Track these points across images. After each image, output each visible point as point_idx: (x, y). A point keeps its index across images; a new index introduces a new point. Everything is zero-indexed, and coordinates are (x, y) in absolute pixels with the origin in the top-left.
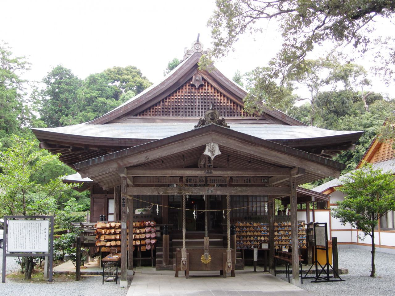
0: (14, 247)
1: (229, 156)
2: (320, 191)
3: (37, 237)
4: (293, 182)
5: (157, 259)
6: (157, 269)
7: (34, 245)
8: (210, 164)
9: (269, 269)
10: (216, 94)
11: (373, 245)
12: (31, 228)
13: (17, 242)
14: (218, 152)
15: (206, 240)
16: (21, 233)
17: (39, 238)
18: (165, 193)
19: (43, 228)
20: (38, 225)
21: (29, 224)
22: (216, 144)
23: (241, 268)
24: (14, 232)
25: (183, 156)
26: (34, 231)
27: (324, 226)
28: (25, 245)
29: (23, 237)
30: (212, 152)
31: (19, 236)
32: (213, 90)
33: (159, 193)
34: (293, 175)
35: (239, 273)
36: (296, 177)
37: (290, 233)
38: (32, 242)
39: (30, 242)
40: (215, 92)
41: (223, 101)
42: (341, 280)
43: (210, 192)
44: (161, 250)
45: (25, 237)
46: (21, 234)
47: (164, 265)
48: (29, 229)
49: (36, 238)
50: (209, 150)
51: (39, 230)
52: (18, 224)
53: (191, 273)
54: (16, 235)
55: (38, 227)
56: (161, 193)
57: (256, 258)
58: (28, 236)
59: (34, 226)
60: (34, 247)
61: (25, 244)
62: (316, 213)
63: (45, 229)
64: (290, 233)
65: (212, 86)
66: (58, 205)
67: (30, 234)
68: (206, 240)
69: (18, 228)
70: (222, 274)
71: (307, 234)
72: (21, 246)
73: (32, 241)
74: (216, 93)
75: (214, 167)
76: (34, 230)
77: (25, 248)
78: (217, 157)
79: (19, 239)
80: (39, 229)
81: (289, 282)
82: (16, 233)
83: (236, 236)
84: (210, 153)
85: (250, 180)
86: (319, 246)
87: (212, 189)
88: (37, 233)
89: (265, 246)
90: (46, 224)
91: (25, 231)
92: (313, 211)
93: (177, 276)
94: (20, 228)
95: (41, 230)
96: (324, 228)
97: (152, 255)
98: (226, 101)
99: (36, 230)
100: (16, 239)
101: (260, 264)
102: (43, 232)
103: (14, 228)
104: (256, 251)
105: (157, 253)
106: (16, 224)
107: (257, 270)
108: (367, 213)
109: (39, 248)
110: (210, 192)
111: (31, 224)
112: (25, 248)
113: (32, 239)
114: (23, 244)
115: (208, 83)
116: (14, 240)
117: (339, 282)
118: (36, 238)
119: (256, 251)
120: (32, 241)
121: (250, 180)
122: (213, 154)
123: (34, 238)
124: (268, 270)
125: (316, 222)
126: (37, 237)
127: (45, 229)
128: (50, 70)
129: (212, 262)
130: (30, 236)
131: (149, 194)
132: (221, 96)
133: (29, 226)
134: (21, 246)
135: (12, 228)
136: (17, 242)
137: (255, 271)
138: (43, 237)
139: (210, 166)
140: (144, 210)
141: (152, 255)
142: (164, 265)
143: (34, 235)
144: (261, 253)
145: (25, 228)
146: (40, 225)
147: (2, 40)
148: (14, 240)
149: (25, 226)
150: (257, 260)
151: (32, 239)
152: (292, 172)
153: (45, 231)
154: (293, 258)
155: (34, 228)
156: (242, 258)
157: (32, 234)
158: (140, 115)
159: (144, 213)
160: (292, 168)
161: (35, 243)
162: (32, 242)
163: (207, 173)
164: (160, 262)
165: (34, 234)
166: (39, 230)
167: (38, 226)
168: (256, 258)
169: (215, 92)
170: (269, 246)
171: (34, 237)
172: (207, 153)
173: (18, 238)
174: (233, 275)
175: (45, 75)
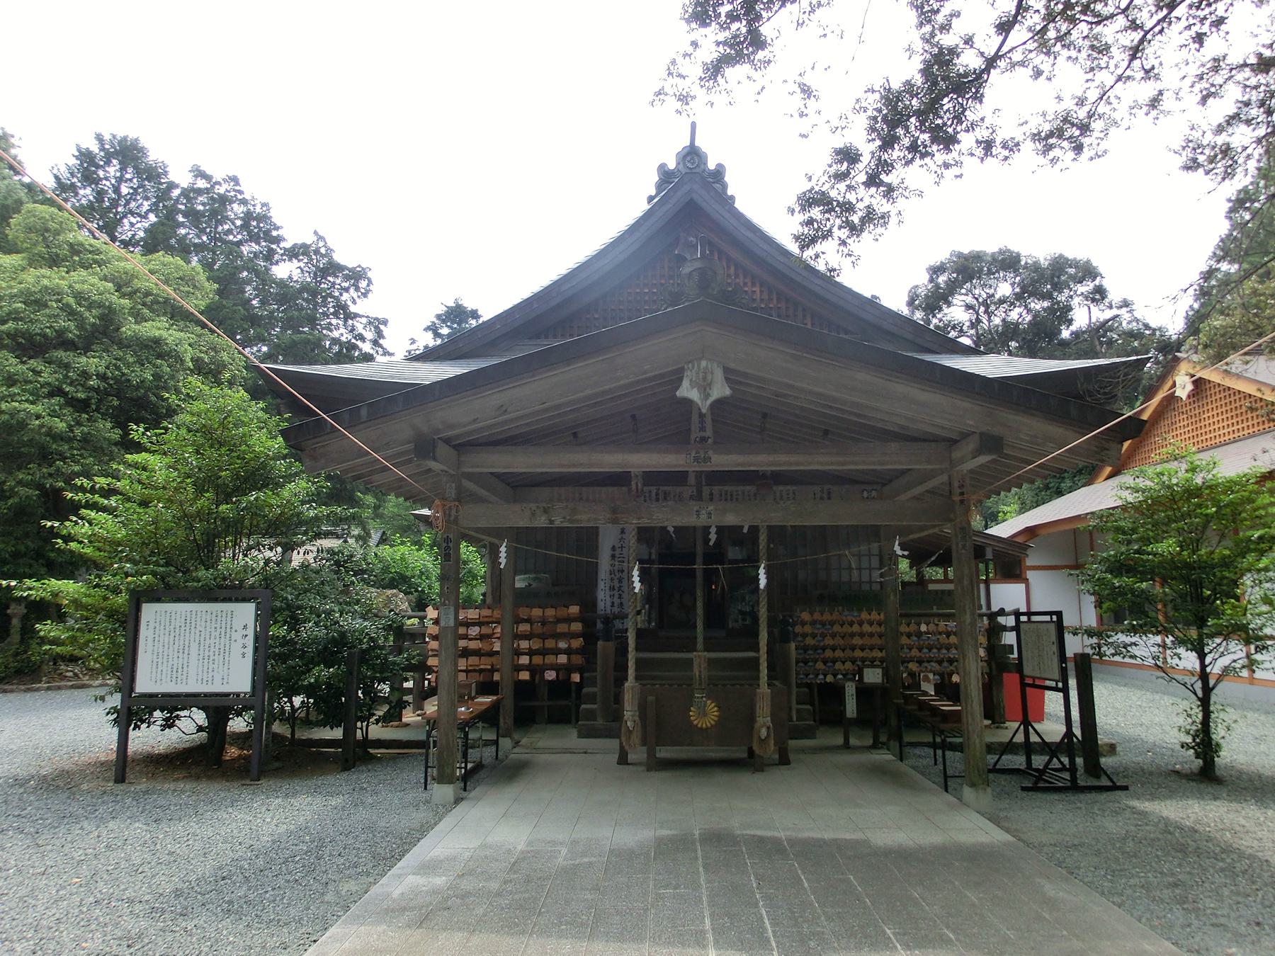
1: (765, 415)
2: (1005, 535)
4: (961, 486)
5: (583, 706)
6: (581, 735)
8: (703, 434)
9: (889, 740)
10: (740, 280)
11: (1204, 676)
14: (720, 390)
15: (700, 658)
18: (570, 521)
19: (238, 625)
22: (715, 365)
23: (807, 733)
25: (633, 417)
27: (1052, 621)
30: (705, 388)
32: (732, 269)
33: (551, 522)
34: (962, 461)
35: (802, 750)
36: (971, 471)
37: (953, 639)
40: (737, 276)
41: (757, 296)
42: (1114, 788)
43: (704, 516)
44: (594, 684)
47: (600, 722)
50: (693, 384)
53: (664, 753)
56: (558, 522)
57: (851, 708)
58: (194, 646)
62: (993, 587)
63: (245, 627)
64: (953, 639)
65: (729, 259)
68: (700, 658)
70: (751, 763)
71: (989, 640)
74: (741, 277)
75: (715, 442)
78: (719, 403)
81: (946, 791)
83: (793, 645)
84: (695, 390)
85: (829, 493)
86: (1034, 678)
87: (711, 508)
89: (873, 676)
90: (245, 613)
92: (987, 582)
93: (623, 760)
96: (1052, 628)
97: (574, 695)
98: (765, 296)
101: (861, 722)
104: (850, 689)
105: (585, 690)
107: (853, 741)
108: (1175, 581)
110: (704, 516)
115: (720, 252)
117: (1104, 796)
119: (850, 689)
121: (829, 493)
122: (707, 396)
124: (883, 739)
125: (995, 608)
127: (245, 627)
128: (441, 310)
129: (721, 722)
131: (521, 524)
132: (753, 284)
135: (152, 625)
137: (846, 746)
138: (236, 649)
139: (703, 440)
140: (535, 579)
141: (574, 695)
142: (600, 722)
144: (865, 693)
150: (855, 715)
152: (956, 455)
154: (964, 720)
156: (812, 704)
157: (207, 642)
158: (546, 337)
159: (534, 585)
160: (955, 442)
161: (215, 666)
163: (696, 459)
164: (591, 715)
168: (851, 708)
169: (737, 276)
170: (886, 674)
172: (687, 391)
174: (784, 760)
175: (430, 318)
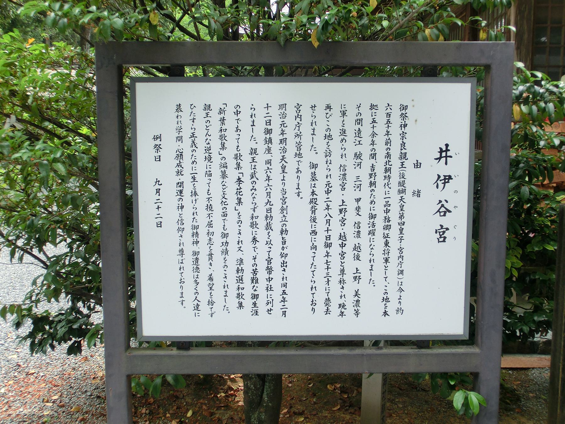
0: (190, 303)
3: (380, 222)
7: (351, 286)
12: (321, 144)
13: (218, 258)
16: (246, 186)
17: (395, 228)
20: (381, 118)
21: (306, 112)
24: (186, 179)
26: (351, 174)
28: (276, 284)
29: (262, 223)
31: (232, 216)
38: (335, 260)
39: (320, 261)
45: (277, 225)
46: (246, 198)
48: (308, 157)
49: (365, 230)
51: (395, 162)
52: (215, 117)
54: (202, 202)
55: (380, 140)
58: (299, 210)
59: (351, 128)
60: (350, 301)
61: (277, 273)
63: (444, 153)
66: (308, 15)
67: (321, 197)
69: (216, 145)
72: (248, 292)
73: (335, 250)
76: (350, 161)
77: (277, 306)
79: (232, 239)
80: (395, 152)
82: (201, 188)
88: (380, 190)
91: (276, 166)
94: (231, 144)
95: (409, 164)
99: (367, 162)
100: (203, 238)
102: (422, 179)
103: (186, 146)
106: (200, 113)
109: (392, 307)
111: (320, 111)
112: (277, 306)
113: (335, 241)
114: (262, 275)
116: (189, 249)
118: (365, 230)
120: (335, 250)
123: (349, 230)
126: (380, 222)
127: (444, 153)
130: (321, 214)
133: (306, 129)
134: (248, 292)
136: (218, 258)
138: (421, 217)
143: (351, 206)
145: (276, 147)
146: (396, 120)
147: (157, 181)
148: (189, 249)
149: (276, 126)
151: (335, 241)
153: (442, 169)
155: (351, 149)
157: (336, 196)
162: (335, 260)
165: (350, 195)
166: (395, 162)
167: (381, 129)
171: (351, 217)
173: (217, 229)
